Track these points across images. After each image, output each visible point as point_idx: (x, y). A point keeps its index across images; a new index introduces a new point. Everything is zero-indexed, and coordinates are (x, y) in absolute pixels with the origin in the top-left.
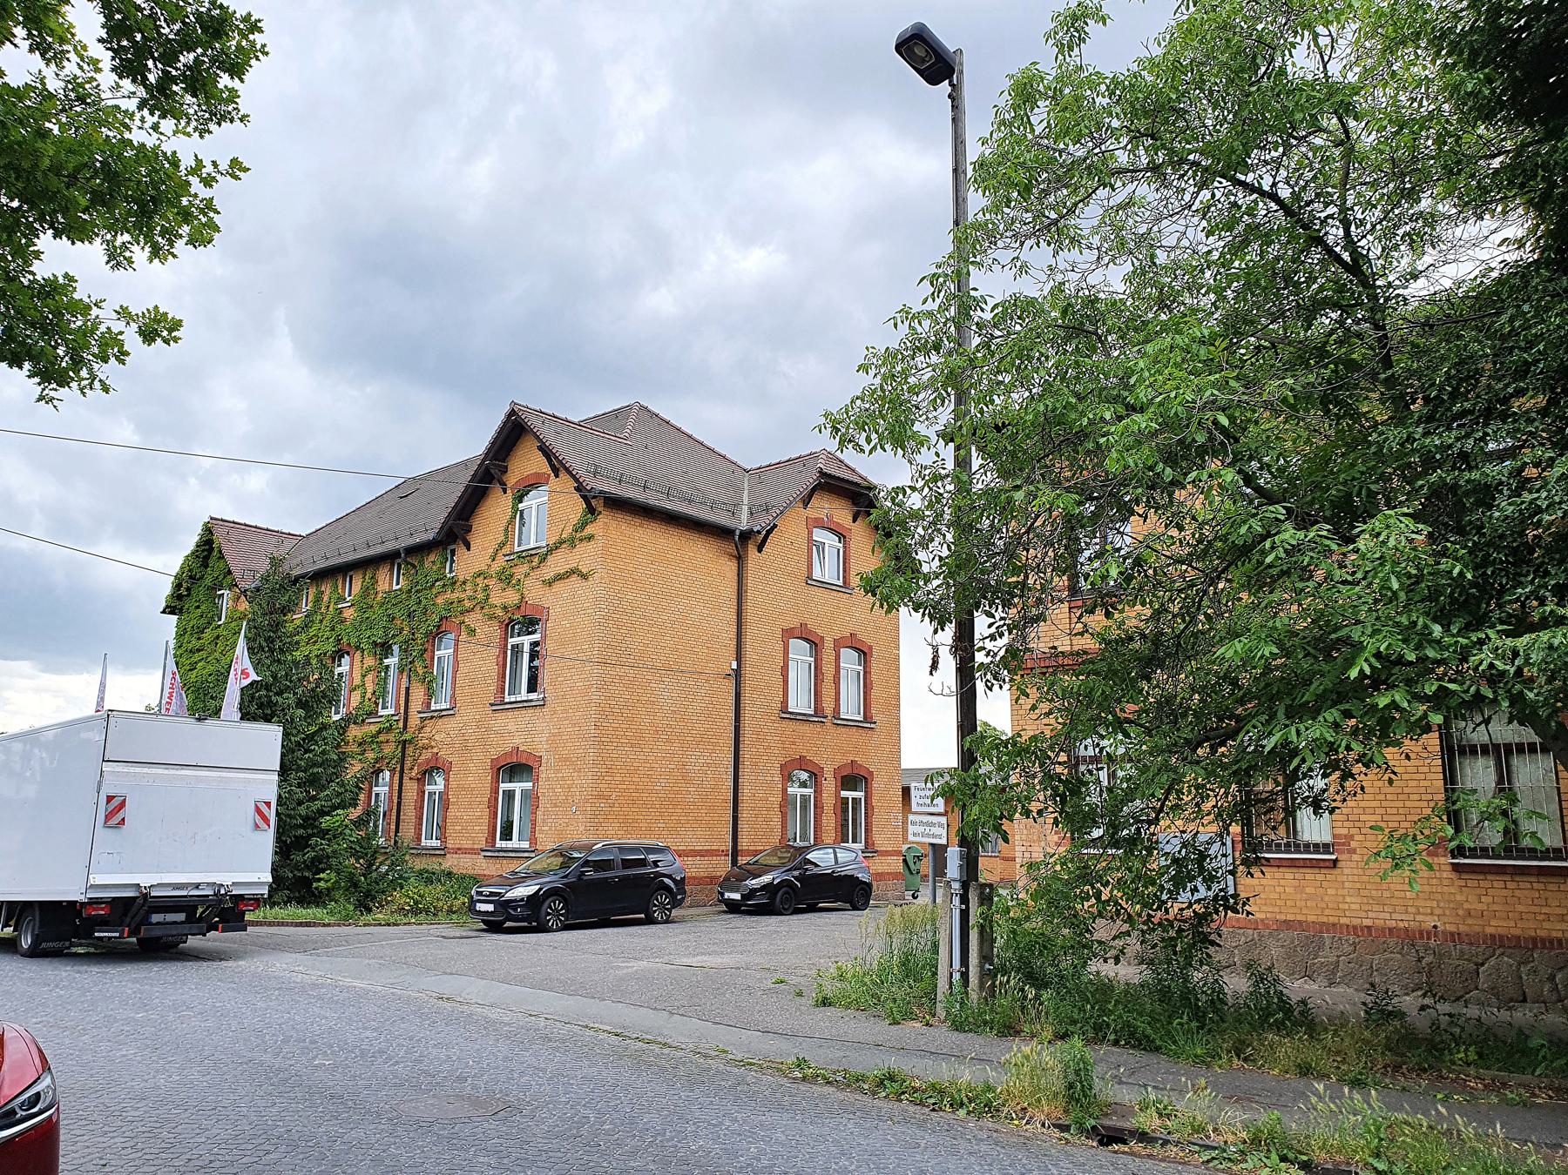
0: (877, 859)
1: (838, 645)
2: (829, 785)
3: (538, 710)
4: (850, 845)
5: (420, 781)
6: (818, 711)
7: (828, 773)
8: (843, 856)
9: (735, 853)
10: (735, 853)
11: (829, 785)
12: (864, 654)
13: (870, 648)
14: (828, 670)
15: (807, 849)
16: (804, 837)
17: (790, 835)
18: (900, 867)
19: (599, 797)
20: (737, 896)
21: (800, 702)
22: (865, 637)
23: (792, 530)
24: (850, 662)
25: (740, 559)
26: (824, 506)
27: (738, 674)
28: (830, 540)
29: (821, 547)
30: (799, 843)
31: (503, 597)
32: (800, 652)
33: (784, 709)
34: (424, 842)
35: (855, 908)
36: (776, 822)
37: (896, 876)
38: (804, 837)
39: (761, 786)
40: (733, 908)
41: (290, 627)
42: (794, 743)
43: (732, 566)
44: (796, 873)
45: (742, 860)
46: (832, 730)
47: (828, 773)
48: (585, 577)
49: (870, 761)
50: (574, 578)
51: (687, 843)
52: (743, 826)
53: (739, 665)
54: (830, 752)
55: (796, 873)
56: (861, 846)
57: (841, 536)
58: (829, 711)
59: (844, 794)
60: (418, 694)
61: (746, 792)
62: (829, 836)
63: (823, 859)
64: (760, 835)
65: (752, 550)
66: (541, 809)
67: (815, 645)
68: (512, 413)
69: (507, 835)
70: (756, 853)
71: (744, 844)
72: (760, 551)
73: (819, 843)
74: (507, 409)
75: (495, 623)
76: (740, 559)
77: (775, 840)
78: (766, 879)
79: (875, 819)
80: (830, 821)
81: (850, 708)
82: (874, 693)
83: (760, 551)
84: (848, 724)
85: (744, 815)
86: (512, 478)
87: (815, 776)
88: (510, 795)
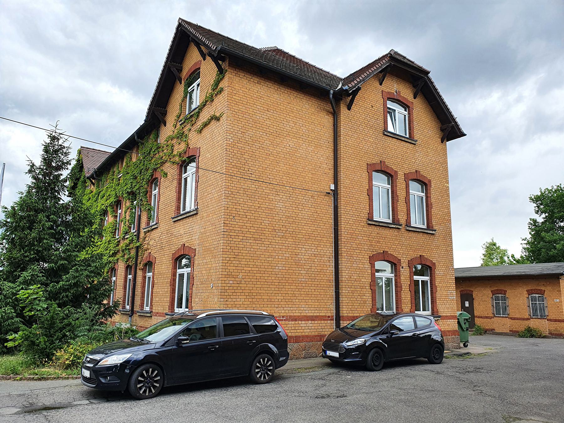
0: (441, 322)
1: (408, 178)
2: (405, 272)
3: (195, 217)
4: (421, 312)
5: (144, 271)
6: (395, 221)
7: (404, 263)
8: (421, 322)
9: (338, 318)
10: (338, 318)
11: (405, 272)
12: (425, 184)
13: (430, 181)
14: (401, 193)
15: (393, 316)
16: (389, 308)
17: (378, 305)
18: (456, 327)
19: (229, 275)
20: (336, 355)
21: (381, 214)
22: (426, 173)
23: (371, 96)
24: (416, 191)
25: (335, 114)
26: (392, 86)
27: (335, 193)
28: (399, 111)
29: (391, 112)
30: (385, 312)
31: (179, 148)
32: (381, 183)
33: (370, 218)
34: (177, 310)
35: (431, 362)
36: (368, 296)
37: (453, 332)
38: (389, 308)
39: (354, 269)
40: (334, 363)
41: (62, 178)
42: (379, 242)
43: (328, 120)
44: (384, 336)
45: (343, 324)
46: (406, 234)
47: (404, 263)
48: (218, 119)
49: (433, 256)
50: (213, 122)
51: (298, 311)
52: (343, 300)
53: (336, 187)
54: (405, 248)
55: (384, 336)
56: (429, 313)
57: (405, 106)
58: (403, 221)
59: (416, 278)
60: (144, 219)
61: (344, 275)
62: (407, 306)
63: (405, 324)
64: (356, 307)
65: (343, 110)
66: (195, 286)
67: (391, 176)
68: (180, 25)
69: (180, 306)
70: (354, 318)
71: (344, 312)
72: (349, 108)
73: (399, 313)
74: (176, 24)
75: (175, 166)
76: (335, 114)
77: (367, 309)
78: (359, 341)
79: (438, 295)
80: (406, 296)
81: (417, 221)
82: (434, 211)
83: (349, 108)
84: (417, 231)
85: (344, 291)
86: (185, 73)
87: (395, 265)
88: (182, 276)
